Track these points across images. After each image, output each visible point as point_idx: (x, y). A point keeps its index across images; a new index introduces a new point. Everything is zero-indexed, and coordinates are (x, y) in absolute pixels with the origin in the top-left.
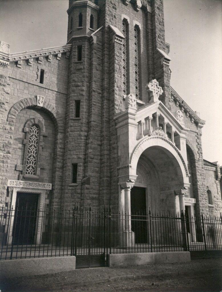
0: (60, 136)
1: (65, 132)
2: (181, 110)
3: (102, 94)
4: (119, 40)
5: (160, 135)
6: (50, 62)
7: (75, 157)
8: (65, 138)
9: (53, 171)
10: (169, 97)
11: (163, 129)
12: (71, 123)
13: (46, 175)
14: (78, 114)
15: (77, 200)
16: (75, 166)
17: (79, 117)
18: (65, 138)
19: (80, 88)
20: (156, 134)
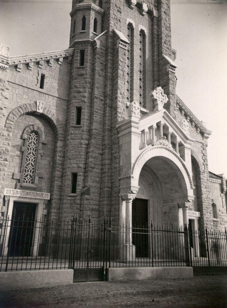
0: (60, 144)
1: (65, 140)
2: (186, 119)
3: (105, 101)
4: (124, 45)
5: (164, 145)
6: (51, 66)
7: (75, 166)
8: (65, 146)
9: (52, 180)
10: (174, 106)
11: (167, 138)
12: (71, 131)
13: (44, 185)
14: (79, 122)
15: (76, 211)
16: (75, 176)
17: (80, 124)
18: (65, 146)
19: (81, 94)
20: (160, 143)
